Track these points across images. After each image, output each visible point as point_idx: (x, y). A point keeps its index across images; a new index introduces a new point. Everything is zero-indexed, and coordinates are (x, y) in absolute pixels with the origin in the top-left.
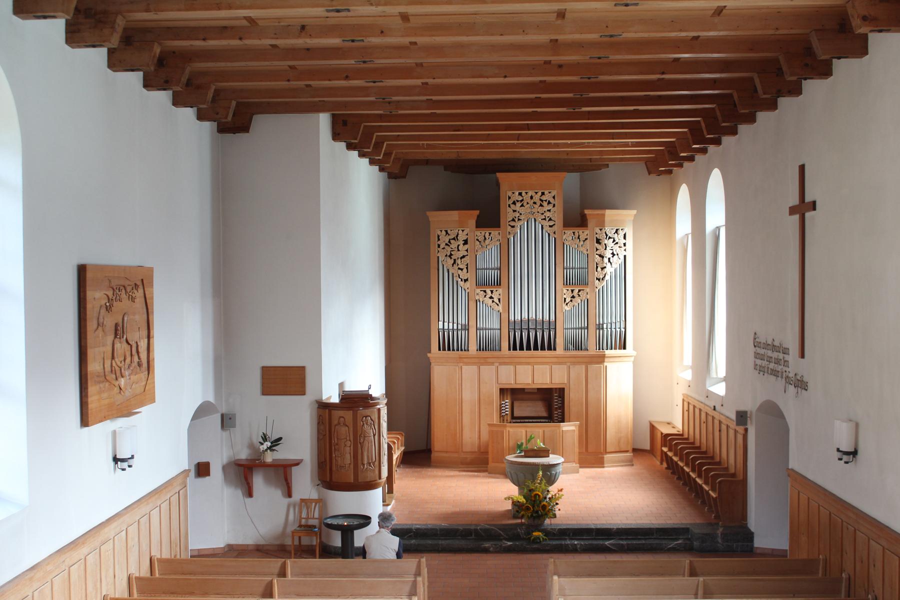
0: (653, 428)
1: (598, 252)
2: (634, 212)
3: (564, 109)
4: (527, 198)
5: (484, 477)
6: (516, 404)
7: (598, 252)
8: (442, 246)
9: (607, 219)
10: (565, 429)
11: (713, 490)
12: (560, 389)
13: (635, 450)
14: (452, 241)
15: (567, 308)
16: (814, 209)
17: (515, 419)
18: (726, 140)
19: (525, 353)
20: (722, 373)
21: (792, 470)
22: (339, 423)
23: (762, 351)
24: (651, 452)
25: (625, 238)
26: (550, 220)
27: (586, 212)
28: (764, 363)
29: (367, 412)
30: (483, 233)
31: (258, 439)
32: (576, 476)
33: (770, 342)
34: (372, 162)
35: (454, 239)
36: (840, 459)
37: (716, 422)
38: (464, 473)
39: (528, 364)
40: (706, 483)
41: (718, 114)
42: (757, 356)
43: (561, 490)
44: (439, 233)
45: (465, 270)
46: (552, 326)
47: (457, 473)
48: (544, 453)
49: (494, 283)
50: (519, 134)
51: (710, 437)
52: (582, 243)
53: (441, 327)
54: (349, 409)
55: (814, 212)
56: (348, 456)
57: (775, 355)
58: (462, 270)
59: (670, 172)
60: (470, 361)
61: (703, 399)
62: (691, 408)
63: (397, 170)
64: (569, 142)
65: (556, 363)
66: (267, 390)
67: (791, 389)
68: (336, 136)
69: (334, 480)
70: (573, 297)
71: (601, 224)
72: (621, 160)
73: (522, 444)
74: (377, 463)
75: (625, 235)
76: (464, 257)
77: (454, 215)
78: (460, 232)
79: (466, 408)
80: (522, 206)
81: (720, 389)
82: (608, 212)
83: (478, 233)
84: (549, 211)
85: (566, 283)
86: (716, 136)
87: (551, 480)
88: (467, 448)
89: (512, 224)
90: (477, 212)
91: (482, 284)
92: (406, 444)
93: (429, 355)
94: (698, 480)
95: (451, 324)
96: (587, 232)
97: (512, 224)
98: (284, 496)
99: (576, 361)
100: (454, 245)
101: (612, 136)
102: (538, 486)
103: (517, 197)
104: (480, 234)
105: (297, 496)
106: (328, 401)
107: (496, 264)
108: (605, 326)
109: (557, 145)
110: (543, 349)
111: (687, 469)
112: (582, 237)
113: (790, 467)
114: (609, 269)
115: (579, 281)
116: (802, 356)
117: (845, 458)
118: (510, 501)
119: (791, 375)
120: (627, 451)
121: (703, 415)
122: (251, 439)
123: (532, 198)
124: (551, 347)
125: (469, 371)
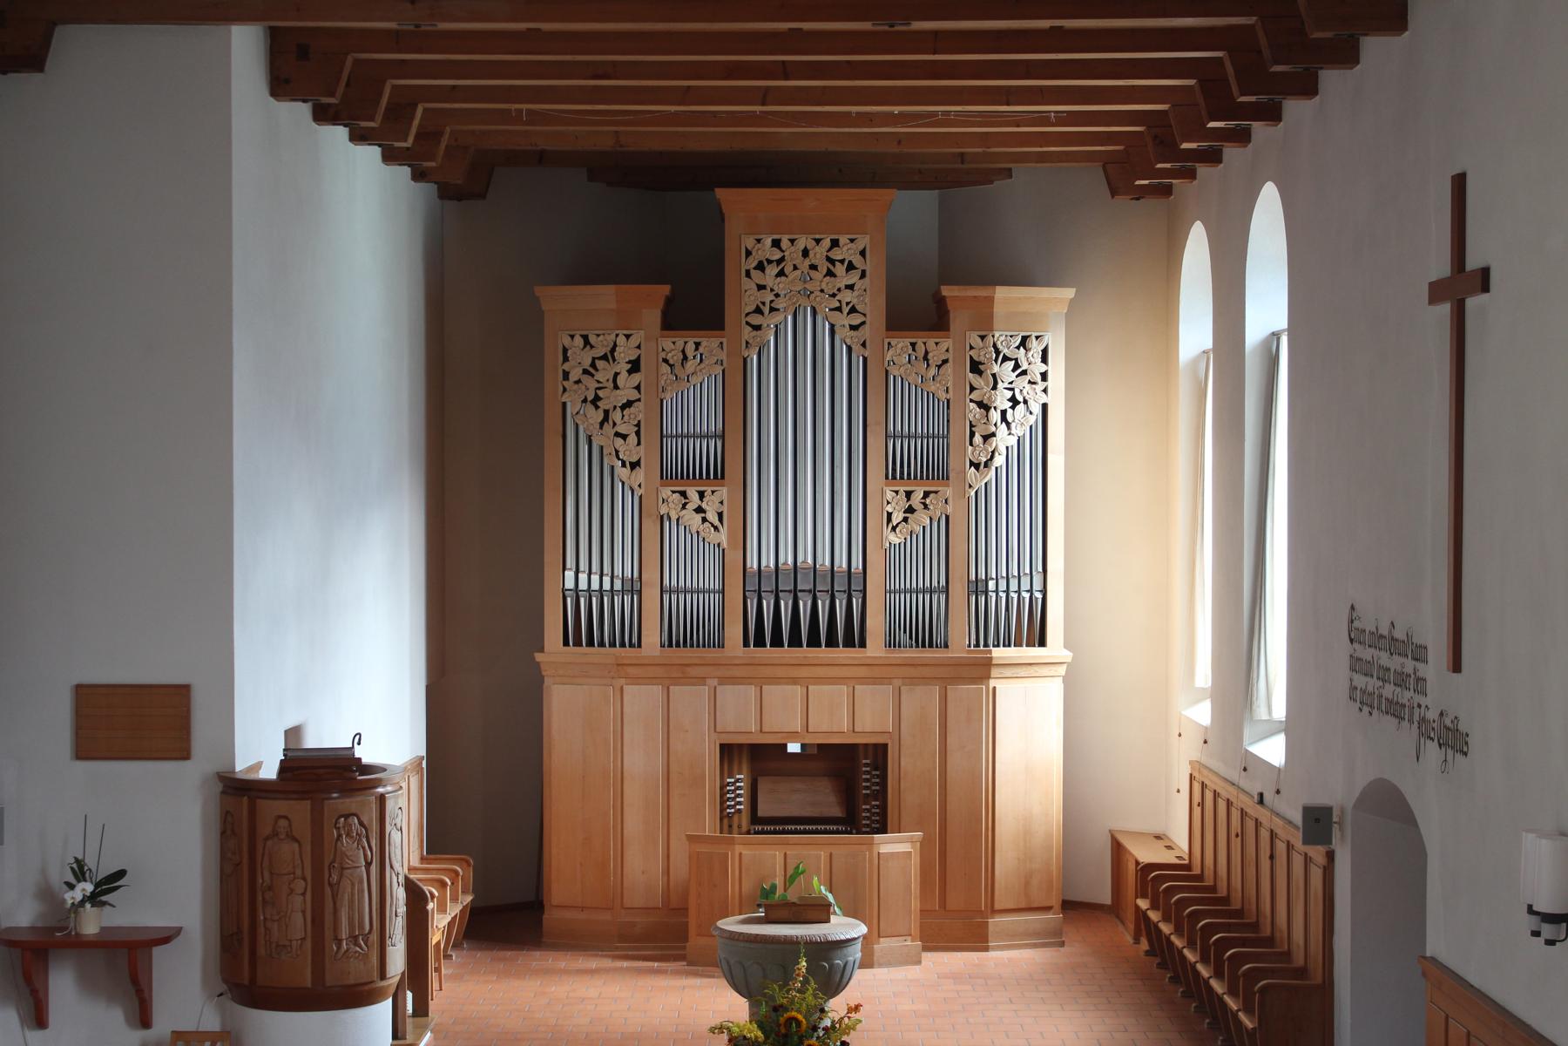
0: (1118, 849)
1: (974, 396)
2: (1069, 293)
3: (866, 26)
4: (792, 253)
5: (678, 973)
6: (764, 785)
7: (974, 396)
8: (574, 376)
9: (999, 310)
10: (884, 849)
11: (1248, 1009)
12: (875, 746)
13: (1068, 906)
14: (600, 364)
15: (895, 539)
16: (1485, 288)
17: (761, 823)
18: (1294, 108)
19: (786, 653)
20: (1280, 711)
21: (1433, 958)
22: (275, 834)
23: (1367, 653)
24: (1114, 909)
25: (1044, 360)
26: (853, 310)
27: (946, 291)
28: (1372, 684)
29: (351, 803)
30: (680, 343)
31: (59, 873)
32: (912, 972)
33: (1384, 631)
34: (389, 157)
35: (605, 357)
36: (1536, 934)
37: (1265, 834)
38: (626, 964)
39: (794, 681)
40: (1232, 992)
41: (1263, 41)
42: (1356, 664)
43: (857, 1008)
44: (567, 341)
45: (632, 439)
46: (855, 584)
47: (607, 963)
48: (817, 911)
49: (709, 470)
50: (767, 89)
51: (1251, 872)
52: (933, 371)
53: (570, 584)
54: (302, 795)
55: (1485, 296)
56: (298, 919)
57: (1394, 663)
58: (624, 437)
59: (1167, 191)
60: (645, 674)
61: (1234, 775)
62: (1209, 796)
63: (460, 176)
64: (896, 110)
65: (863, 680)
66: (85, 749)
67: (1432, 750)
68: (281, 86)
69: (330, 980)
70: (910, 510)
71: (985, 325)
72: (1042, 158)
73: (774, 887)
74: (374, 937)
75: (1045, 353)
76: (629, 404)
77: (605, 296)
78: (621, 340)
79: (633, 793)
80: (781, 273)
81: (1273, 751)
82: (1002, 293)
83: (667, 343)
84: (850, 287)
85: (893, 475)
86: (1264, 98)
87: (833, 983)
88: (636, 898)
89: (756, 320)
90: (666, 289)
91: (676, 475)
92: (480, 885)
93: (539, 657)
94: (1214, 983)
95: (595, 578)
96: (946, 343)
97: (756, 320)
98: (130, 1022)
99: (917, 676)
100: (604, 373)
101: (1008, 96)
102: (798, 996)
103: (766, 251)
104: (672, 345)
105: (166, 1020)
106: (252, 776)
107: (714, 425)
108: (991, 585)
109: (869, 119)
110: (832, 642)
111: (1190, 956)
112: (935, 358)
113: (1428, 954)
114: (1004, 440)
115: (926, 468)
116: (1457, 666)
117: (1548, 930)
118: (725, 1037)
119: (1432, 715)
120: (1048, 909)
121: (1235, 815)
122: (44, 872)
123: (805, 253)
124: (855, 638)
125: (641, 699)
